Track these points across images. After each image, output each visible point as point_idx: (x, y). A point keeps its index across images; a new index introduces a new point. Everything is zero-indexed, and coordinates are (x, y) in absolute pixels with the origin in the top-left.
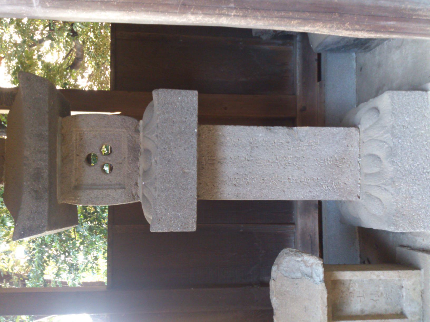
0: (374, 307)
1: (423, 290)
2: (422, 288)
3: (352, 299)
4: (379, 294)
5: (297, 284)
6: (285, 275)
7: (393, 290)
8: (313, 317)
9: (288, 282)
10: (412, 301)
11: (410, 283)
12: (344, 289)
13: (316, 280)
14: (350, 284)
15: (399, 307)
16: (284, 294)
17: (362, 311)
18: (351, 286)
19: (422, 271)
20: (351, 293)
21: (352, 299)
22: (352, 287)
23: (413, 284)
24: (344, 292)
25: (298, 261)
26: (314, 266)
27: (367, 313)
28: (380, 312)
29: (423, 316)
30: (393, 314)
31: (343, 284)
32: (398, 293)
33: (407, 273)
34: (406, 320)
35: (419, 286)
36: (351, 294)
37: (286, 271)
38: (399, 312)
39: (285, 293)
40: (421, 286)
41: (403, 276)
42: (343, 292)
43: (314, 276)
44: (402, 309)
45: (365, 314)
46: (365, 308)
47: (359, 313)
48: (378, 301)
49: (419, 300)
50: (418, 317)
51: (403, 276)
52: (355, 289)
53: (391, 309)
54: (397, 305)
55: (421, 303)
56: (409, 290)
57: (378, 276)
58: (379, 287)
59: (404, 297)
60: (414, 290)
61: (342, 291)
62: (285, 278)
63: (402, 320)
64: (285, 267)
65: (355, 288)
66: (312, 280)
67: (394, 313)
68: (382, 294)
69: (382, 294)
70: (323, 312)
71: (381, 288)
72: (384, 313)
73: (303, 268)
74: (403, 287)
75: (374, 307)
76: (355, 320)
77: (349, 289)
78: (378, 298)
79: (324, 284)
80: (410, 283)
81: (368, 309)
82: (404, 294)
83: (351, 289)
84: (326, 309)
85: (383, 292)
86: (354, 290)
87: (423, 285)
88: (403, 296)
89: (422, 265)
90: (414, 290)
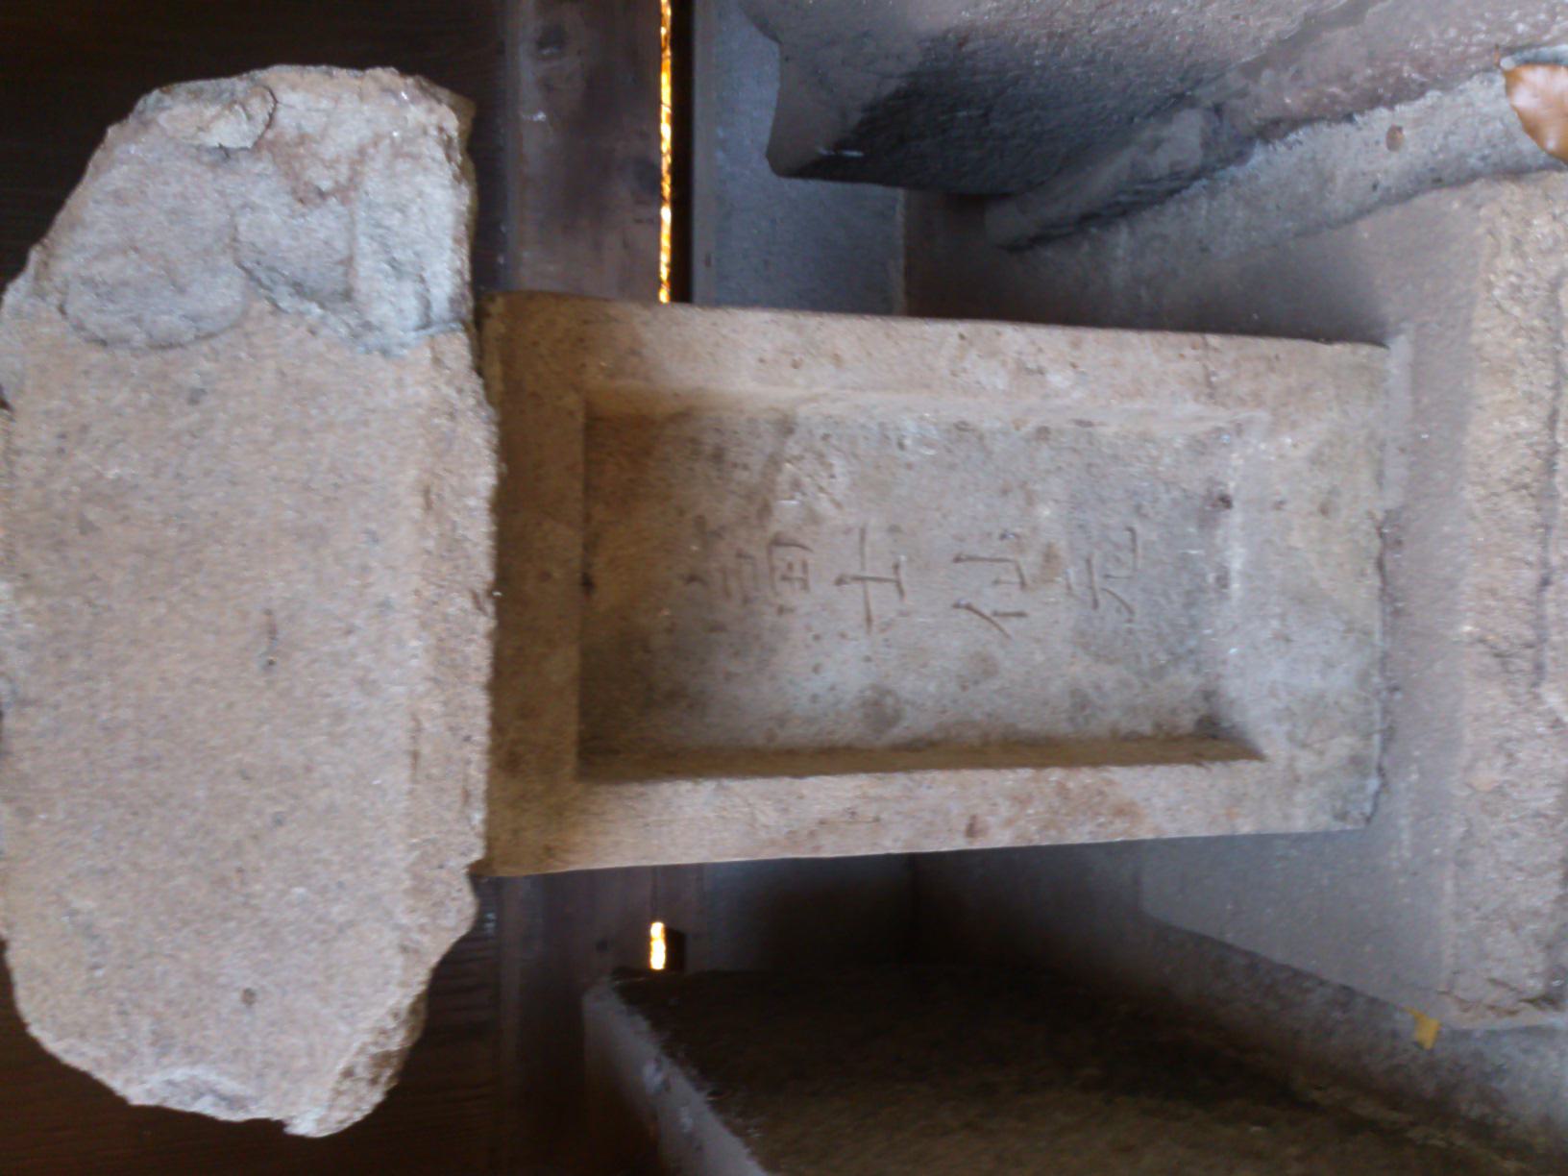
0: (986, 667)
1: (1391, 517)
2: (1393, 498)
3: (791, 595)
4: (1030, 562)
5: (195, 398)
6: (93, 322)
7: (1146, 533)
8: (339, 716)
9: (121, 396)
10: (1305, 600)
11: (1295, 445)
12: (727, 510)
13: (381, 312)
14: (775, 462)
15: (1186, 680)
16: (86, 527)
17: (879, 708)
18: (783, 480)
19: (1401, 348)
20: (777, 542)
21: (791, 595)
22: (796, 485)
23: (1316, 460)
24: (718, 534)
25: (226, 153)
26: (374, 183)
27: (915, 723)
28: (1029, 723)
29: (1389, 736)
30: (1137, 738)
31: (718, 456)
32: (1184, 561)
33: (1272, 363)
34: (1248, 768)
35: (1365, 476)
36: (793, 555)
37: (107, 292)
38: (1187, 721)
39: (93, 514)
40: (1379, 478)
41: (1244, 388)
42: (707, 533)
43: (369, 270)
44: (1208, 695)
45: (898, 733)
46: (908, 685)
47: (850, 730)
48: (1010, 625)
49: (1362, 597)
50: (1343, 746)
51: (1244, 388)
52: (824, 506)
53: (1119, 696)
54: (1176, 659)
55: (1377, 626)
56: (1279, 505)
57: (1028, 372)
58: (1031, 499)
59: (1236, 586)
60: (1324, 511)
61: (700, 522)
62: (97, 356)
63: (1217, 768)
64: (103, 254)
65: (823, 499)
66: (339, 325)
67: (1146, 727)
68: (1049, 556)
69: (1049, 556)
70: (443, 653)
71: (1045, 512)
72: (1063, 728)
73: (269, 215)
74: (1226, 502)
75: (986, 667)
76: (799, 773)
77: (765, 510)
78: (1016, 600)
79: (458, 348)
80: (1295, 445)
81: (926, 695)
82: (1237, 559)
83: (788, 509)
84: (485, 623)
85: (1062, 545)
86: (814, 518)
87: (1397, 469)
88: (1223, 581)
89: (1390, 309)
90: (1324, 511)
